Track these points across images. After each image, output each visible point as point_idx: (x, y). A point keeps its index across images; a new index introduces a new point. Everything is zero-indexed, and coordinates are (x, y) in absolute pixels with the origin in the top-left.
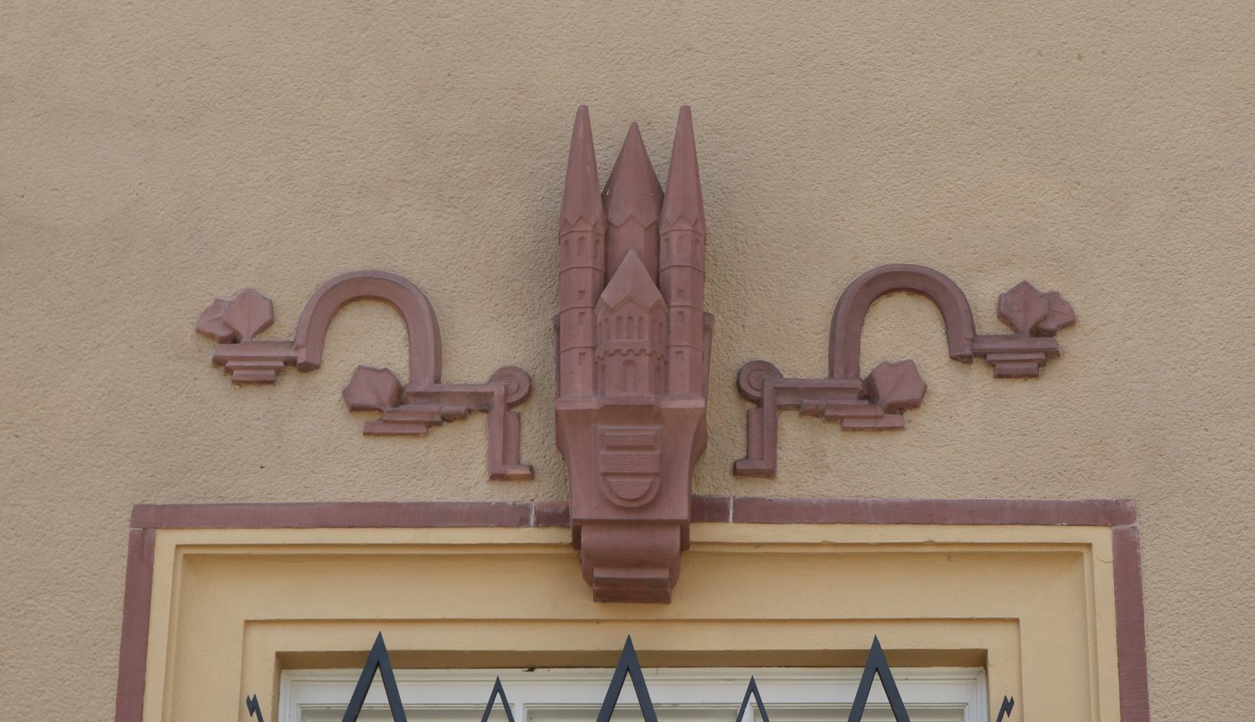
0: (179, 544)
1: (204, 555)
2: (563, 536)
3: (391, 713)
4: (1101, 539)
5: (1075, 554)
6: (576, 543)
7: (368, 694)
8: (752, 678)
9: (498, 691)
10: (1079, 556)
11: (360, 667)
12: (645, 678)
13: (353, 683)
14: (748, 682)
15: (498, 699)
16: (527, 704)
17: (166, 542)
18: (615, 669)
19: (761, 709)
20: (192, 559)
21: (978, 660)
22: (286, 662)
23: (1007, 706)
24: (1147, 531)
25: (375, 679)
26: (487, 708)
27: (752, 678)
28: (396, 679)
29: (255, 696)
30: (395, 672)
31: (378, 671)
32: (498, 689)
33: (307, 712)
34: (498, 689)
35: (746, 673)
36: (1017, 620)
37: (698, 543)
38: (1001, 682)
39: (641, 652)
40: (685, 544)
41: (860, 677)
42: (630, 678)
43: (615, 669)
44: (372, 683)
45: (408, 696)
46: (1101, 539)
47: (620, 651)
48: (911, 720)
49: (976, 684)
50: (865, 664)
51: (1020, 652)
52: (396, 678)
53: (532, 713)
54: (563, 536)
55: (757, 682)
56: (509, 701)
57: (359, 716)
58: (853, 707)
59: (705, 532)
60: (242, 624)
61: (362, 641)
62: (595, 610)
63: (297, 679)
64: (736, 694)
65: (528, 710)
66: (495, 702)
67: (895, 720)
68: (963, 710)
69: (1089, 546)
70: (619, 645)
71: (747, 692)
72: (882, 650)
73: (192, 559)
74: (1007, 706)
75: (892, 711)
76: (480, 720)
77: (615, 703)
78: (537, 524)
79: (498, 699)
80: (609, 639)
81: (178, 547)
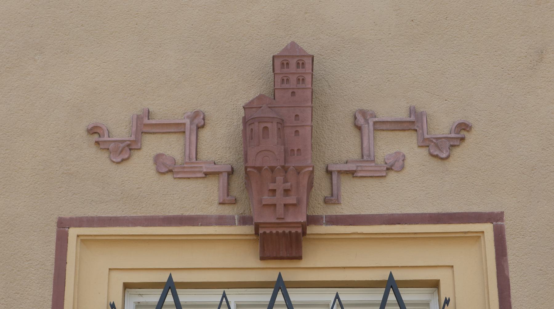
0: (79, 234)
1: (87, 239)
2: (249, 229)
3: (175, 306)
4: (488, 228)
5: (478, 236)
6: (257, 233)
7: (166, 298)
8: (337, 292)
9: (224, 296)
10: (479, 237)
11: (163, 288)
12: (400, 292)
13: (220, 295)
14: (335, 295)
15: (224, 300)
16: (135, 302)
17: (73, 232)
18: (273, 289)
19: (341, 304)
20: (83, 240)
21: (435, 285)
22: (127, 286)
23: (447, 302)
24: (508, 224)
25: (169, 293)
26: (220, 303)
27: (337, 292)
28: (289, 293)
29: (449, 298)
30: (177, 290)
31: (170, 290)
32: (224, 296)
33: (138, 305)
34: (224, 296)
35: (221, 291)
36: (452, 267)
37: (309, 234)
38: (445, 291)
39: (397, 281)
40: (304, 233)
41: (384, 292)
42: (171, 293)
43: (273, 289)
44: (168, 295)
45: (183, 299)
46: (488, 228)
47: (165, 282)
48: (344, 308)
49: (434, 295)
50: (274, 287)
51: (109, 279)
52: (178, 293)
53: (237, 306)
54: (249, 229)
55: (339, 295)
56: (229, 300)
57: (274, 306)
58: (269, 303)
59: (312, 230)
60: (108, 270)
61: (163, 278)
62: (253, 261)
63: (132, 293)
64: (332, 298)
65: (237, 304)
66: (276, 301)
67: (399, 308)
68: (429, 303)
69: (483, 232)
70: (275, 278)
71: (222, 298)
72: (395, 281)
73: (83, 240)
74: (447, 302)
75: (286, 305)
76: (379, 308)
77: (164, 301)
78: (240, 224)
79: (224, 300)
80: (272, 276)
81: (78, 236)
